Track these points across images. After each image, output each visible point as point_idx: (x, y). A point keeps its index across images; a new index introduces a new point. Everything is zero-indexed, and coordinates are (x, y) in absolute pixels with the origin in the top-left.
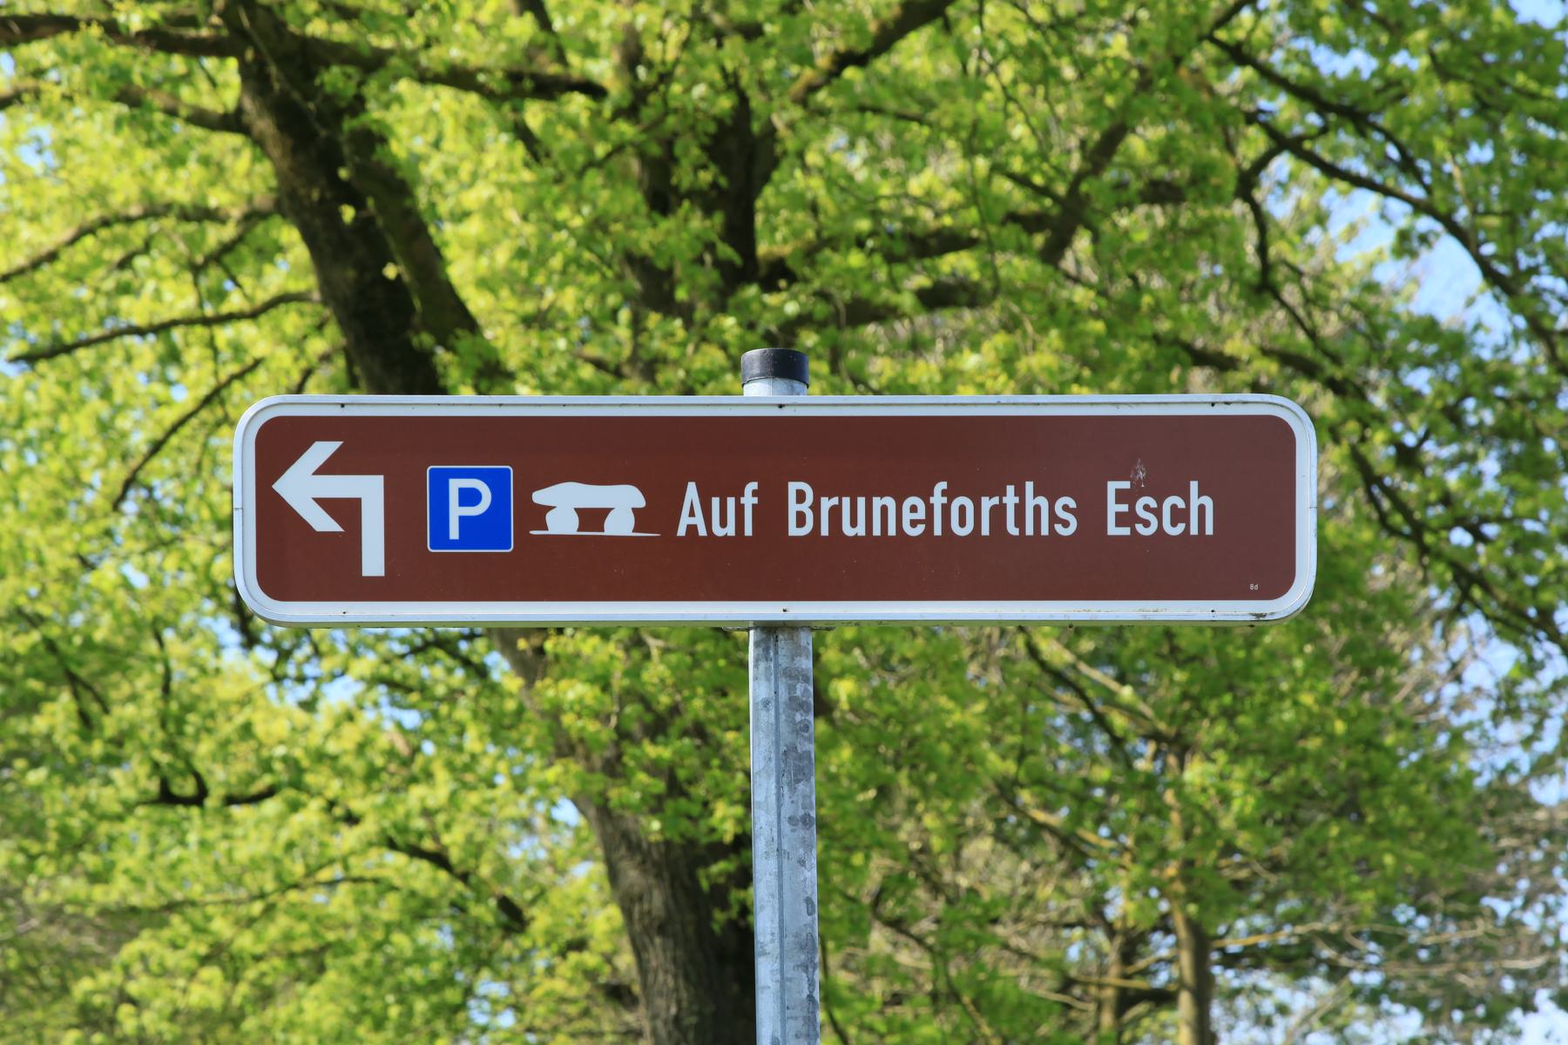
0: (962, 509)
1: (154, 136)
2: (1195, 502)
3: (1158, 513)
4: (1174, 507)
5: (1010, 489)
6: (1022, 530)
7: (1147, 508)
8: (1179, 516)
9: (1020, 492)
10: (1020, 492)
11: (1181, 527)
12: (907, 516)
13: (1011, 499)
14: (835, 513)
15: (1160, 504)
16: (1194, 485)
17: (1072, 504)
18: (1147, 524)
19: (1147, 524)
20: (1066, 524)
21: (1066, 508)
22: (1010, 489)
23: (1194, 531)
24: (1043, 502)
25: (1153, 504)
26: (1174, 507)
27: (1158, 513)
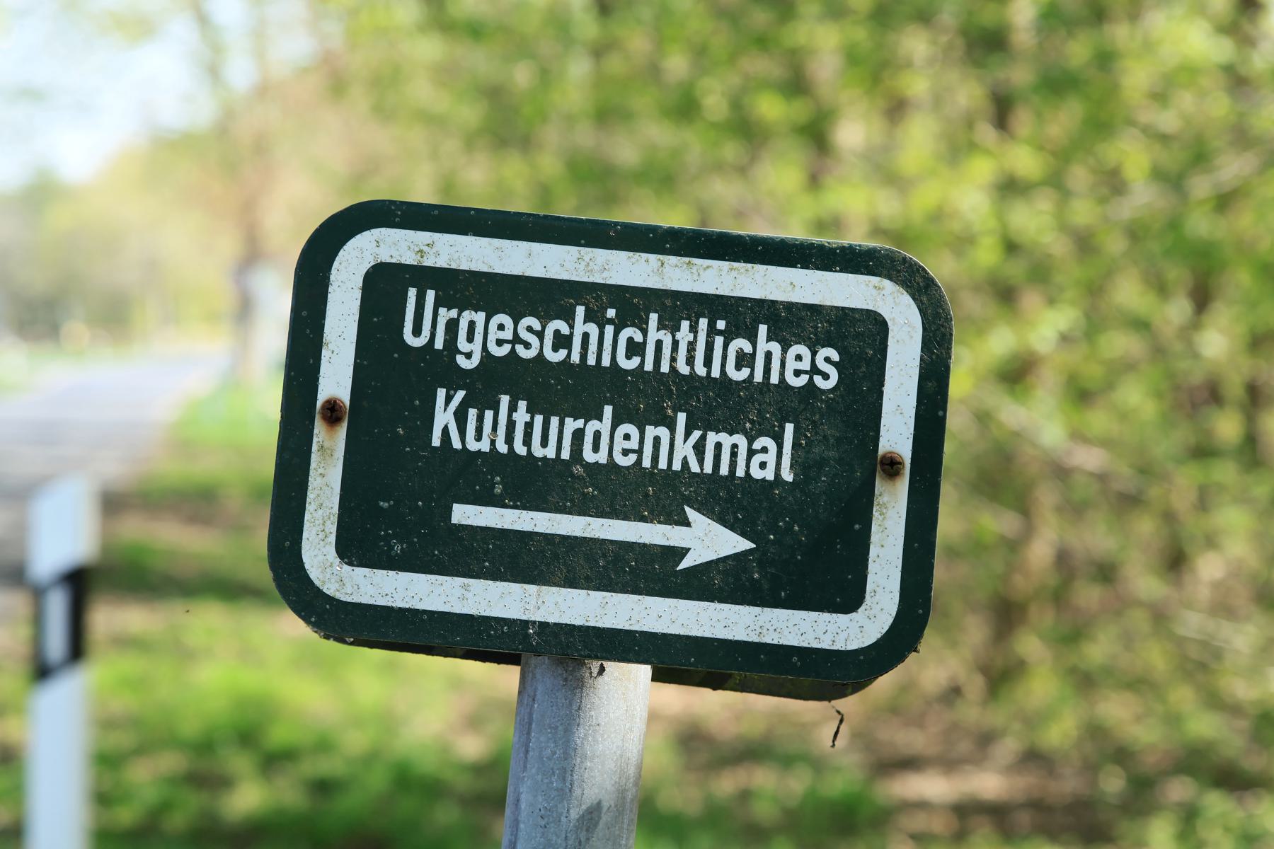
0: (472, 325)
1: (1020, 75)
2: (653, 335)
3: (540, 335)
4: (557, 332)
5: (685, 325)
6: (709, 373)
7: (530, 329)
8: (562, 341)
9: (694, 329)
10: (694, 329)
11: (562, 354)
12: (791, 365)
13: (684, 334)
14: (452, 326)
15: (544, 328)
16: (654, 317)
17: (835, 356)
18: (527, 345)
19: (527, 345)
20: (826, 377)
21: (827, 360)
22: (685, 325)
23: (758, 377)
24: (775, 348)
25: (537, 325)
26: (557, 332)
27: (540, 335)
